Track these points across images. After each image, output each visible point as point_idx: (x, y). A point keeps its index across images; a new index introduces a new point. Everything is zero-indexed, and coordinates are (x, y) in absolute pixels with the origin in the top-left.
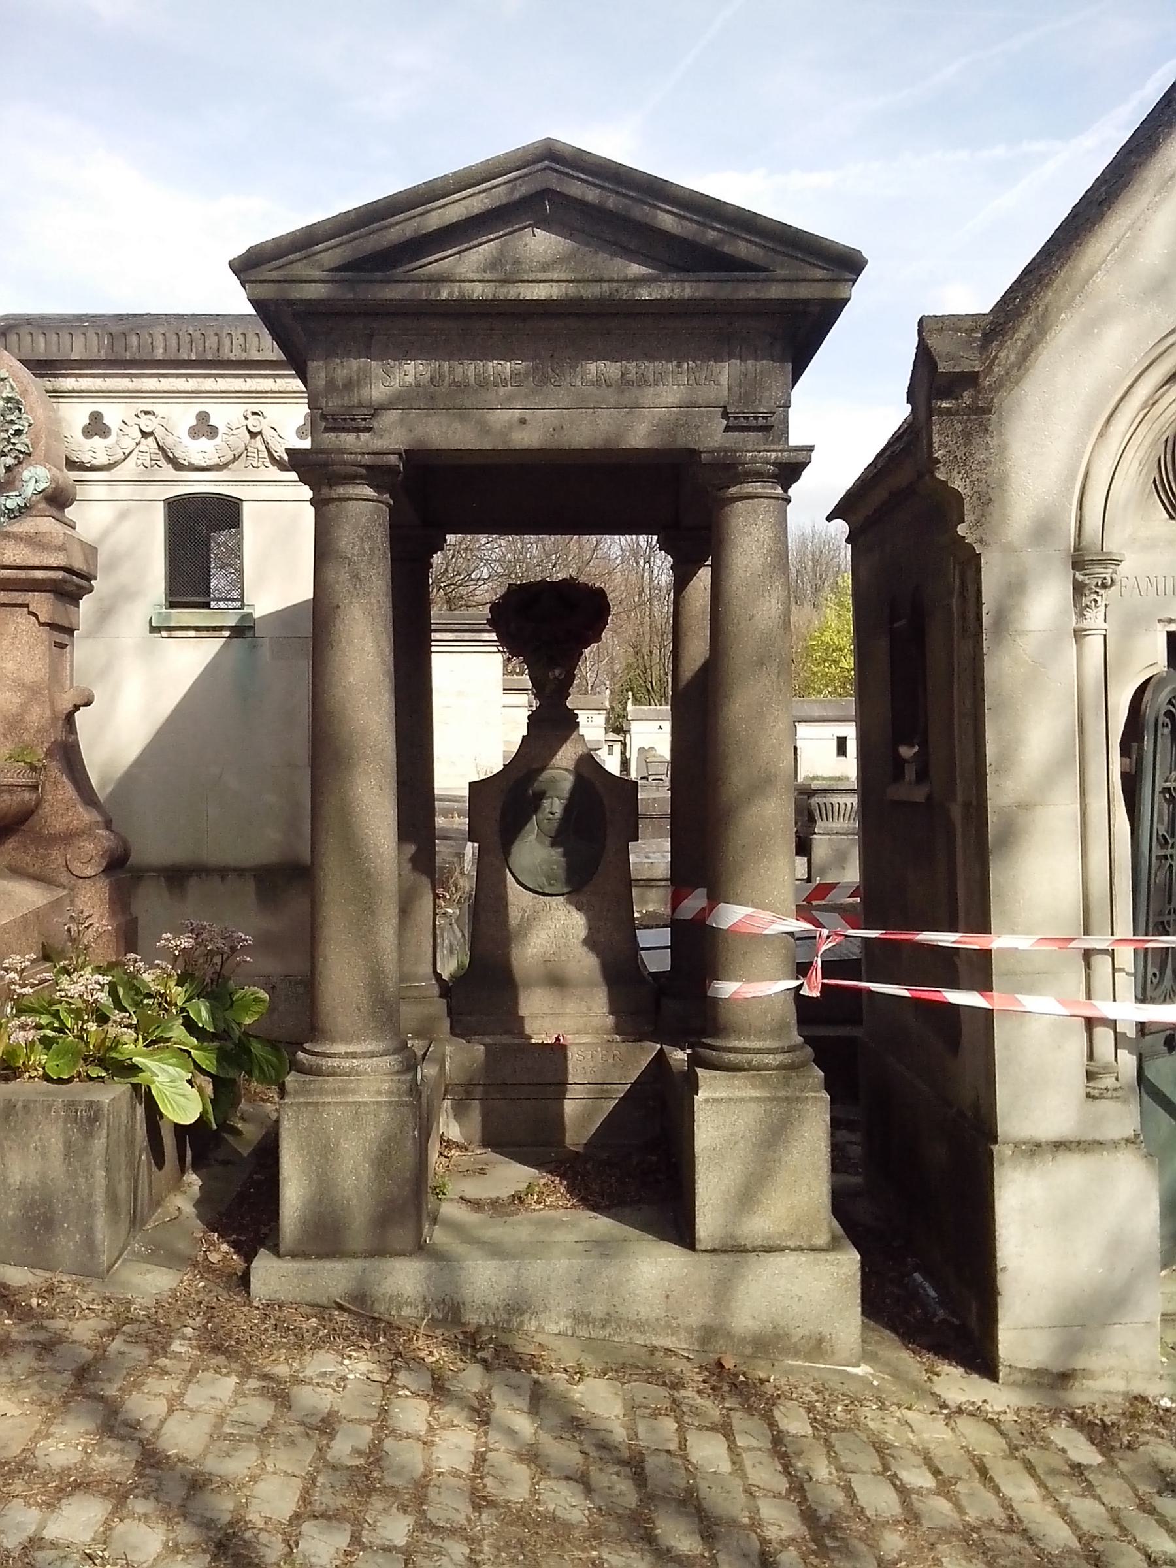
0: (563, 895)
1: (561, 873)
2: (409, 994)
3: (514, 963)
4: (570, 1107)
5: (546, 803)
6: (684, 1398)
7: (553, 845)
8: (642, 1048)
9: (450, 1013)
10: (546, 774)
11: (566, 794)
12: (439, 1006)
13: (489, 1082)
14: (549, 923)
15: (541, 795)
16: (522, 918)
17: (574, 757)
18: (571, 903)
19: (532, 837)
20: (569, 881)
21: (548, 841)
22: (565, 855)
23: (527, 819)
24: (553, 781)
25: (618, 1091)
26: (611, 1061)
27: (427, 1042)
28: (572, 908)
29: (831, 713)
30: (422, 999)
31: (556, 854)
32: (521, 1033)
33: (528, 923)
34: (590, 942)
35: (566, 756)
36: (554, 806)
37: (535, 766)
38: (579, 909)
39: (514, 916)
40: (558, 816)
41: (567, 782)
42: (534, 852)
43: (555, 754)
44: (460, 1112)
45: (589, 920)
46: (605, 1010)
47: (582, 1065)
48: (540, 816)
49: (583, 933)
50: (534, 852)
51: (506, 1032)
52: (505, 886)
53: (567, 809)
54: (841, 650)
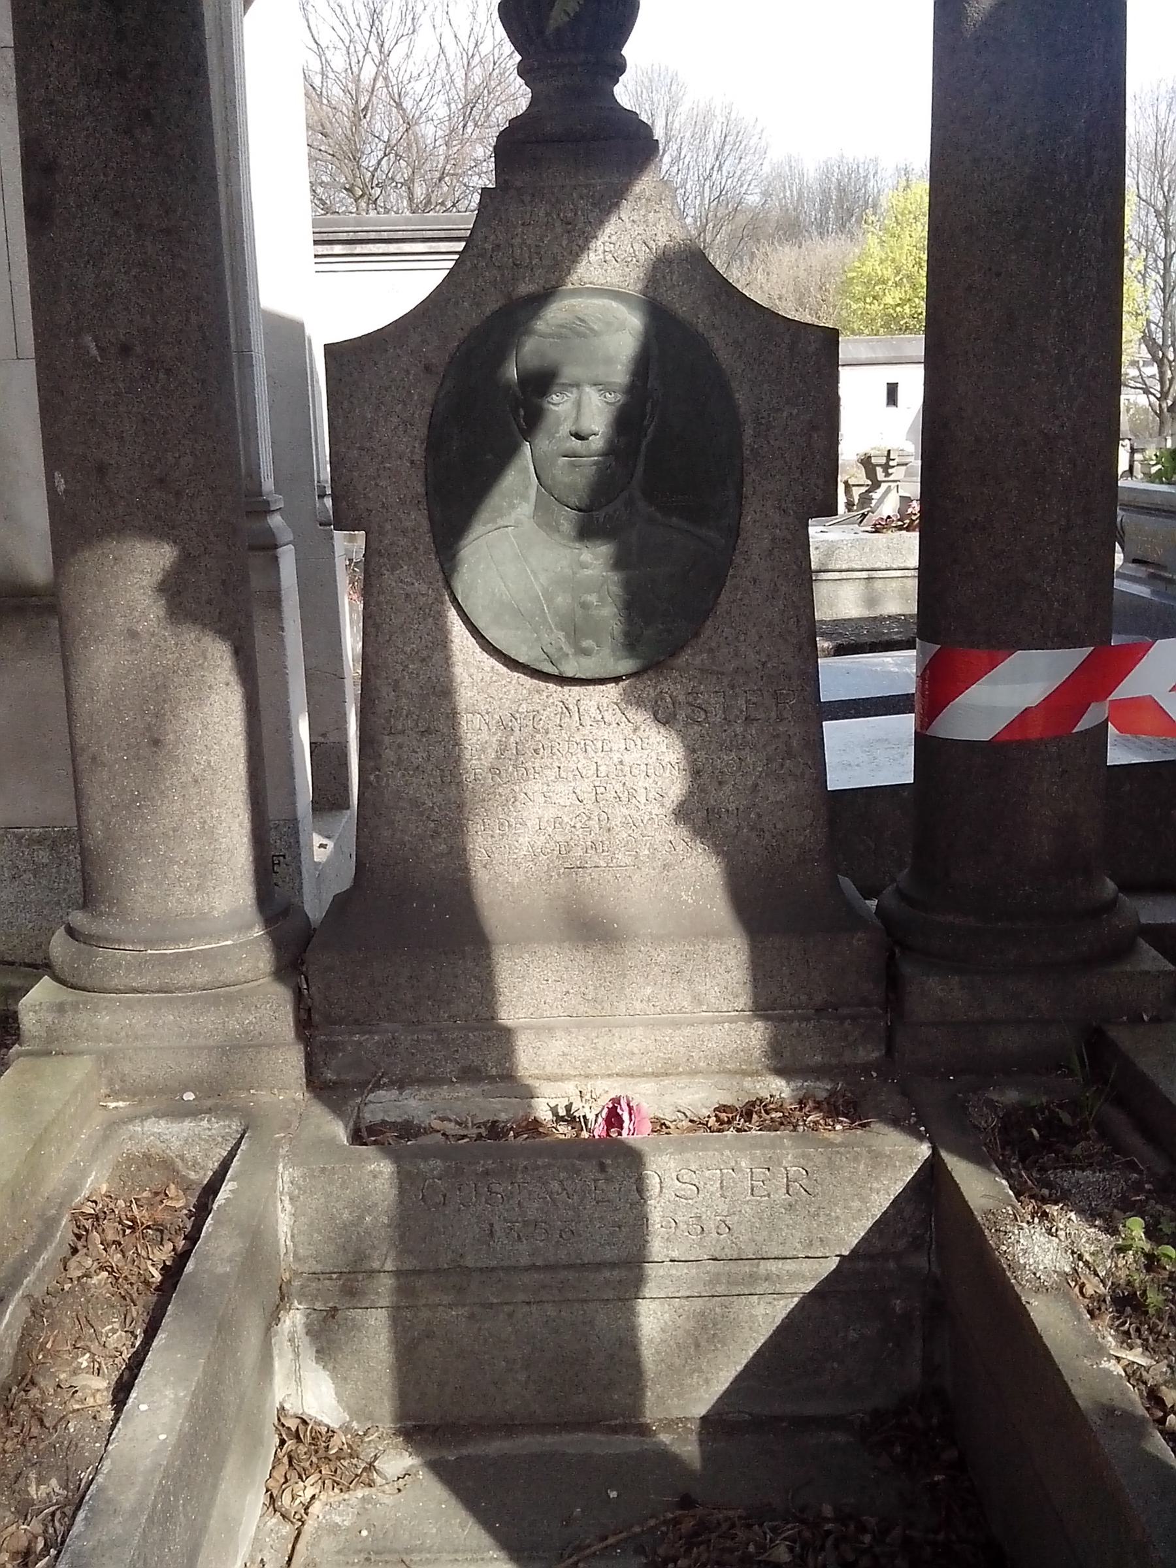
0: (617, 680)
1: (608, 613)
2: (182, 978)
3: (481, 876)
4: (654, 1318)
5: (560, 405)
6: (697, 1093)
7: (586, 532)
8: (876, 1156)
9: (305, 1025)
10: (555, 313)
11: (620, 374)
12: (274, 1011)
13: (411, 1263)
14: (581, 761)
15: (542, 382)
16: (502, 749)
17: (644, 254)
18: (639, 703)
19: (525, 510)
20: (631, 643)
21: (567, 519)
22: (619, 563)
23: (506, 456)
24: (578, 331)
25: (802, 1278)
26: (781, 1195)
27: (235, 1126)
28: (640, 717)
29: (880, 354)
30: (220, 995)
31: (594, 560)
32: (507, 1080)
33: (515, 755)
34: (698, 814)
35: (615, 258)
36: (585, 412)
37: (525, 288)
38: (664, 718)
39: (477, 735)
40: (597, 443)
41: (621, 335)
42: (525, 558)
43: (584, 248)
44: (327, 1337)
45: (691, 750)
46: (743, 1001)
47: (690, 1200)
48: (543, 443)
49: (675, 787)
50: (525, 558)
51: (471, 1075)
52: (447, 661)
53: (626, 421)
54: (884, 283)
